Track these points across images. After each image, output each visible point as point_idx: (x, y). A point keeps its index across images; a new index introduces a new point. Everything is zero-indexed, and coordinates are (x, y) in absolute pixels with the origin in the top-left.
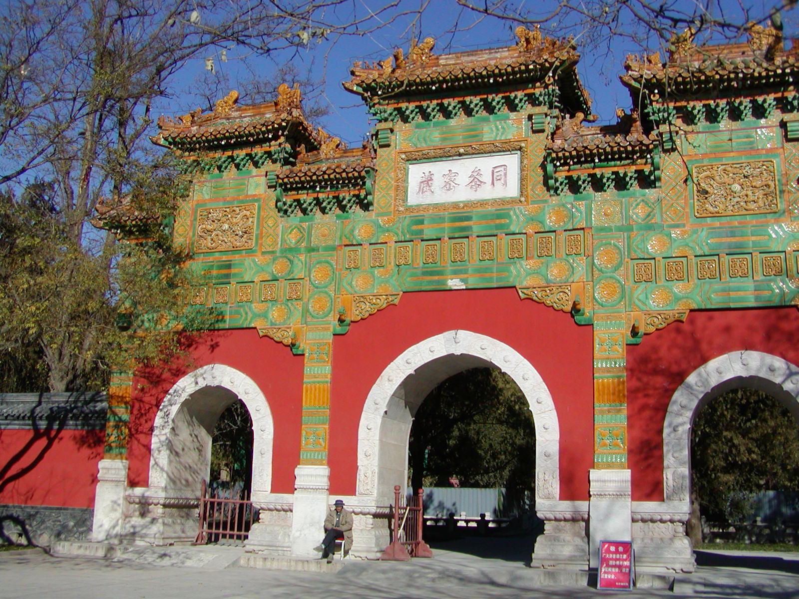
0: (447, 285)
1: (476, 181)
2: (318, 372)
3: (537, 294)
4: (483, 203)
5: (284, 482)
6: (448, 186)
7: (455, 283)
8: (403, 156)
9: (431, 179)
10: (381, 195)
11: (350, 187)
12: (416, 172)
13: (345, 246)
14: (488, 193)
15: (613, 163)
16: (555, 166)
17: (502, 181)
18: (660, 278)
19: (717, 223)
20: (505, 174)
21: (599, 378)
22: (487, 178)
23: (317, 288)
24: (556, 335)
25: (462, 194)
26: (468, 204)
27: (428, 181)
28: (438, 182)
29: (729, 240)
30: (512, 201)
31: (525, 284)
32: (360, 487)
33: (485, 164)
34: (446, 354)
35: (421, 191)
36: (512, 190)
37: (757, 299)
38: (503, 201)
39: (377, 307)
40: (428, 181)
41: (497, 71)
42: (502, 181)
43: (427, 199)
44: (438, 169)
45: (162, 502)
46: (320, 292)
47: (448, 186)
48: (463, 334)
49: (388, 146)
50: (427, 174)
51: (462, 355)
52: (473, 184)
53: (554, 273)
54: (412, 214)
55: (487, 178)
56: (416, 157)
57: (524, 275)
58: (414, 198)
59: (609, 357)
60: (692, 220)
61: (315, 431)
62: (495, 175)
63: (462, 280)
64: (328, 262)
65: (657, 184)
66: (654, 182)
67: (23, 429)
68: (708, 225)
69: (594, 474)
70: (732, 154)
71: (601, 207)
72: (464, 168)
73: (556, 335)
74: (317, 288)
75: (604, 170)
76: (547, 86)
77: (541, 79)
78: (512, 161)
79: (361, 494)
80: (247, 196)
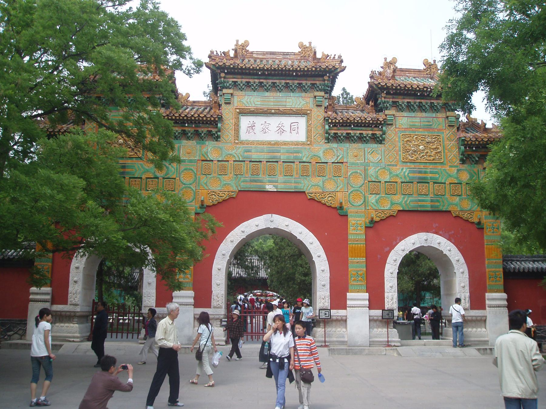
0: (265, 188)
1: (280, 130)
3: (318, 197)
4: (285, 143)
6: (264, 131)
7: (270, 187)
8: (238, 110)
9: (254, 126)
10: (227, 134)
12: (245, 121)
13: (202, 160)
14: (287, 137)
15: (360, 128)
16: (330, 126)
17: (296, 131)
19: (412, 166)
20: (298, 128)
21: (350, 244)
23: (184, 184)
24: (328, 219)
25: (272, 136)
26: (277, 143)
28: (258, 128)
30: (303, 144)
31: (311, 191)
32: (214, 303)
33: (287, 121)
35: (248, 132)
36: (302, 137)
37: (432, 207)
38: (297, 143)
40: (252, 127)
41: (298, 69)
42: (296, 131)
43: (251, 137)
44: (259, 121)
46: (186, 187)
47: (264, 131)
48: (276, 217)
49: (230, 103)
50: (252, 122)
52: (279, 131)
53: (330, 187)
54: (244, 146)
55: (287, 128)
57: (311, 185)
58: (244, 136)
59: (356, 232)
62: (292, 127)
63: (274, 186)
64: (191, 170)
65: (383, 142)
66: (381, 141)
67: (73, 333)
68: (408, 166)
70: (421, 130)
72: (274, 122)
73: (328, 219)
74: (184, 184)
75: (355, 132)
76: (324, 80)
77: (322, 76)
78: (302, 121)
79: (215, 307)
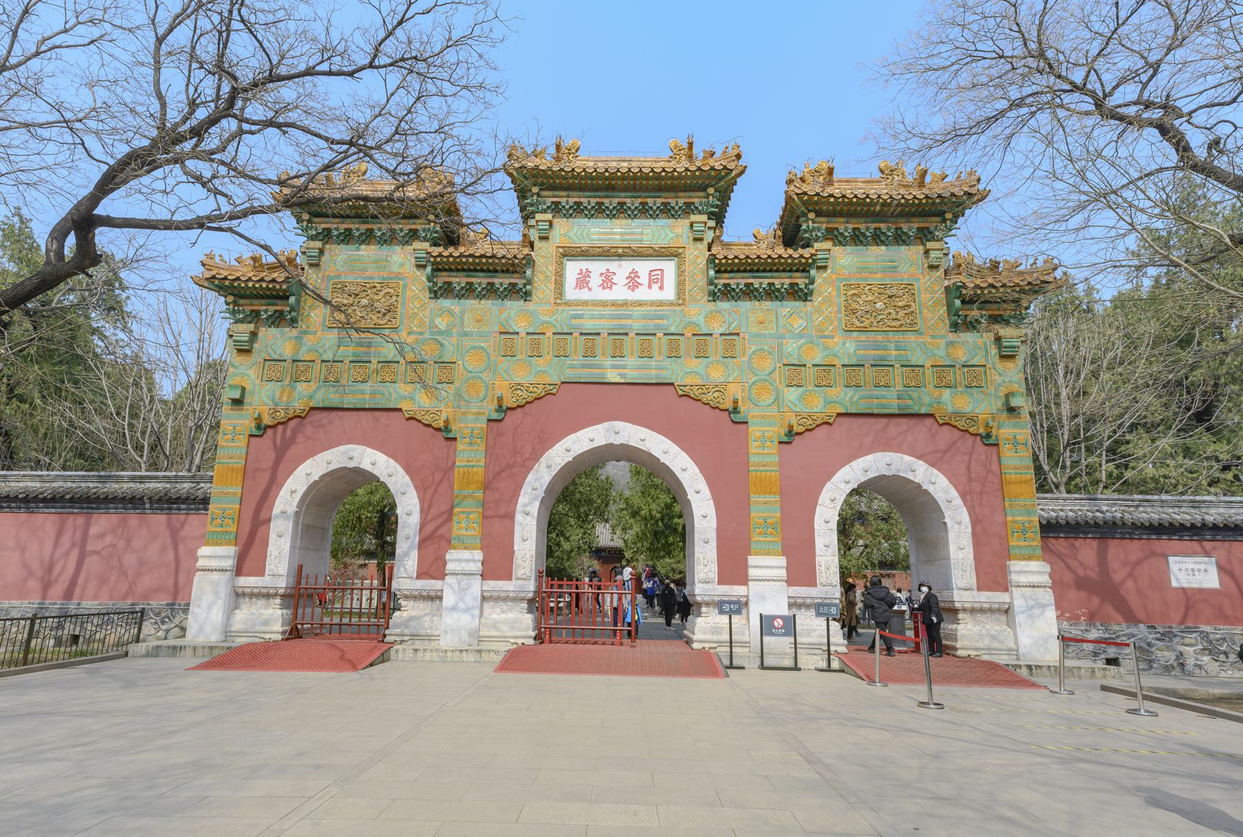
2: (470, 457)
5: (433, 568)
10: (542, 288)
11: (505, 276)
12: (573, 269)
14: (644, 293)
18: (622, 327)
19: (863, 337)
22: (644, 279)
25: (620, 292)
27: (583, 281)
28: (595, 280)
29: (873, 352)
34: (604, 443)
36: (669, 293)
39: (534, 395)
40: (583, 281)
44: (597, 268)
45: (281, 591)
48: (619, 425)
51: (622, 445)
53: (717, 375)
55: (644, 279)
56: (571, 253)
60: (840, 332)
61: (466, 523)
69: (752, 560)
71: (748, 316)
72: (622, 269)
79: (518, 579)
80: (391, 273)
